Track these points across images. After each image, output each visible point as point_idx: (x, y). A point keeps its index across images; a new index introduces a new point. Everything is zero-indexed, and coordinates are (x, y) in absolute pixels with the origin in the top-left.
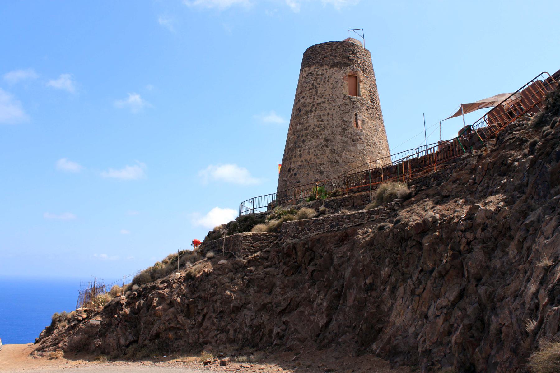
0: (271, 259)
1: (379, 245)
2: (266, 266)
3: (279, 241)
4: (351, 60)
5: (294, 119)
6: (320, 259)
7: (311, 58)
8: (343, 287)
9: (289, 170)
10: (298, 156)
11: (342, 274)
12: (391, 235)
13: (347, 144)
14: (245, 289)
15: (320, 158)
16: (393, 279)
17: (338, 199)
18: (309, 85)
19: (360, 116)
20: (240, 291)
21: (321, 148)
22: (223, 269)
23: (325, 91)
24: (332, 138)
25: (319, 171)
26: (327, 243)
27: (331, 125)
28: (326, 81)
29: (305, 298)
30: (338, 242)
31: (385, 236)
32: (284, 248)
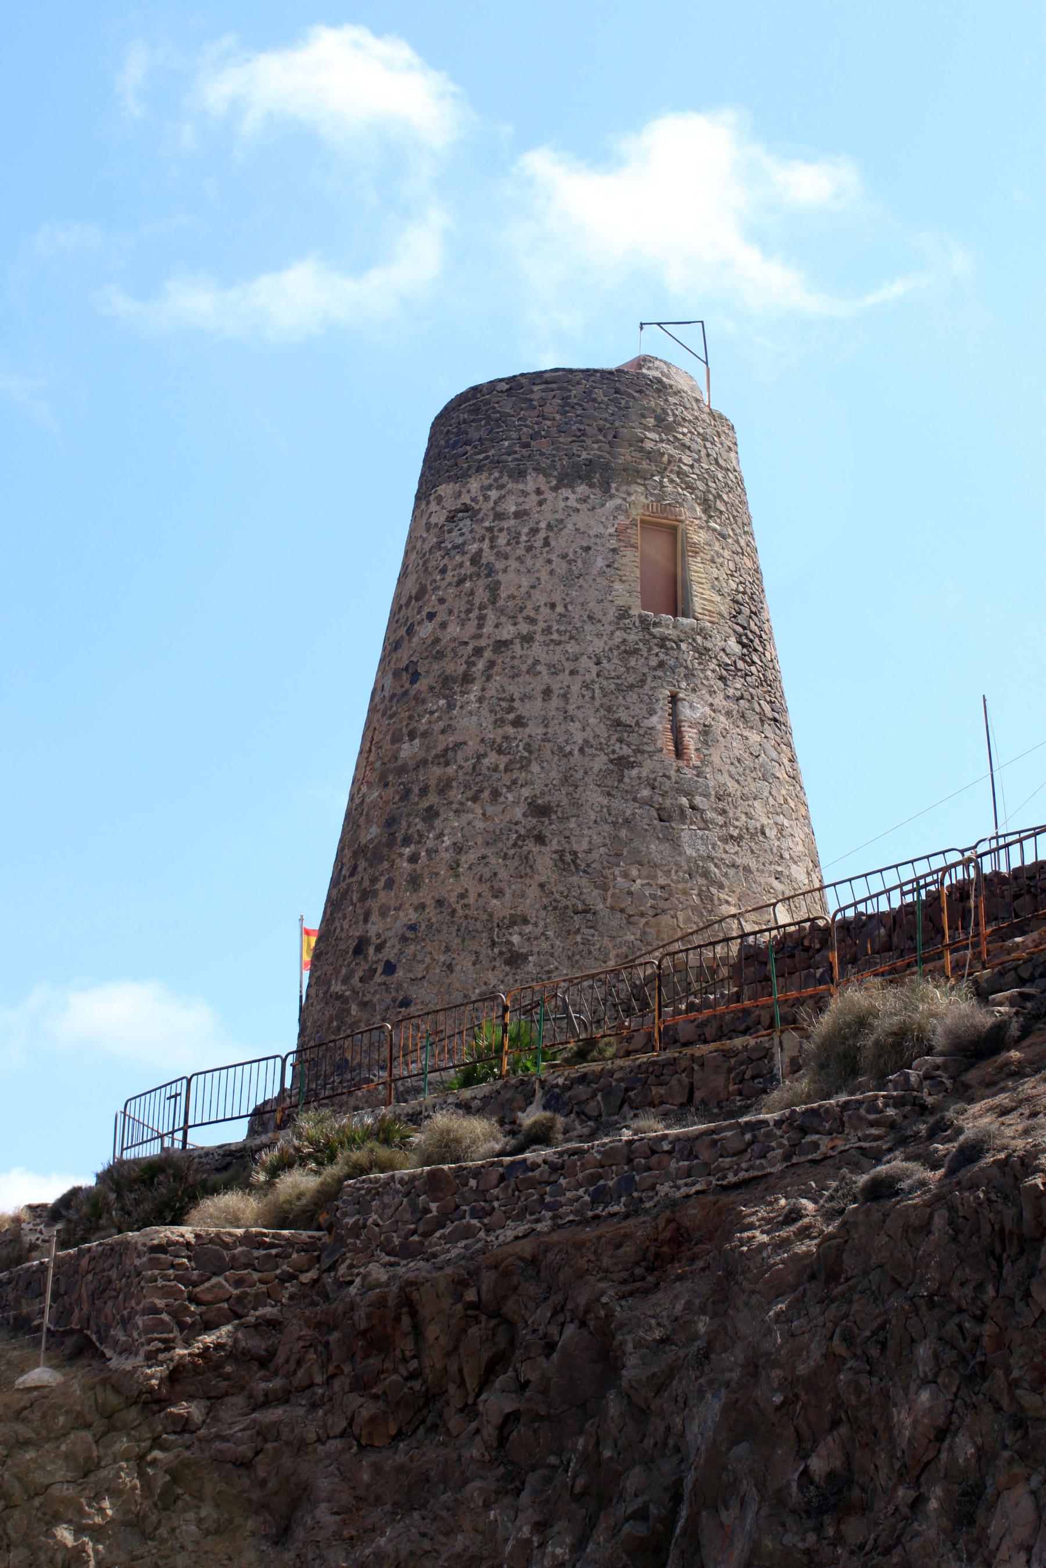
0: (287, 1361)
1: (875, 1276)
2: (262, 1399)
3: (329, 1270)
4: (653, 456)
5: (384, 714)
6: (542, 1359)
7: (467, 443)
8: (677, 1498)
9: (360, 948)
10: (402, 881)
11: (668, 1429)
12: (939, 1220)
13: (632, 830)
14: (154, 1518)
15: (507, 891)
16: (965, 1448)
17: (611, 1072)
18: (458, 558)
19: (691, 707)
20: (128, 1524)
21: (515, 845)
22: (43, 1417)
23: (533, 587)
24: (565, 802)
25: (501, 953)
26: (580, 1275)
27: (561, 740)
28: (539, 544)
29: (472, 1558)
30: (639, 1271)
31: (906, 1228)
32: (352, 1307)
